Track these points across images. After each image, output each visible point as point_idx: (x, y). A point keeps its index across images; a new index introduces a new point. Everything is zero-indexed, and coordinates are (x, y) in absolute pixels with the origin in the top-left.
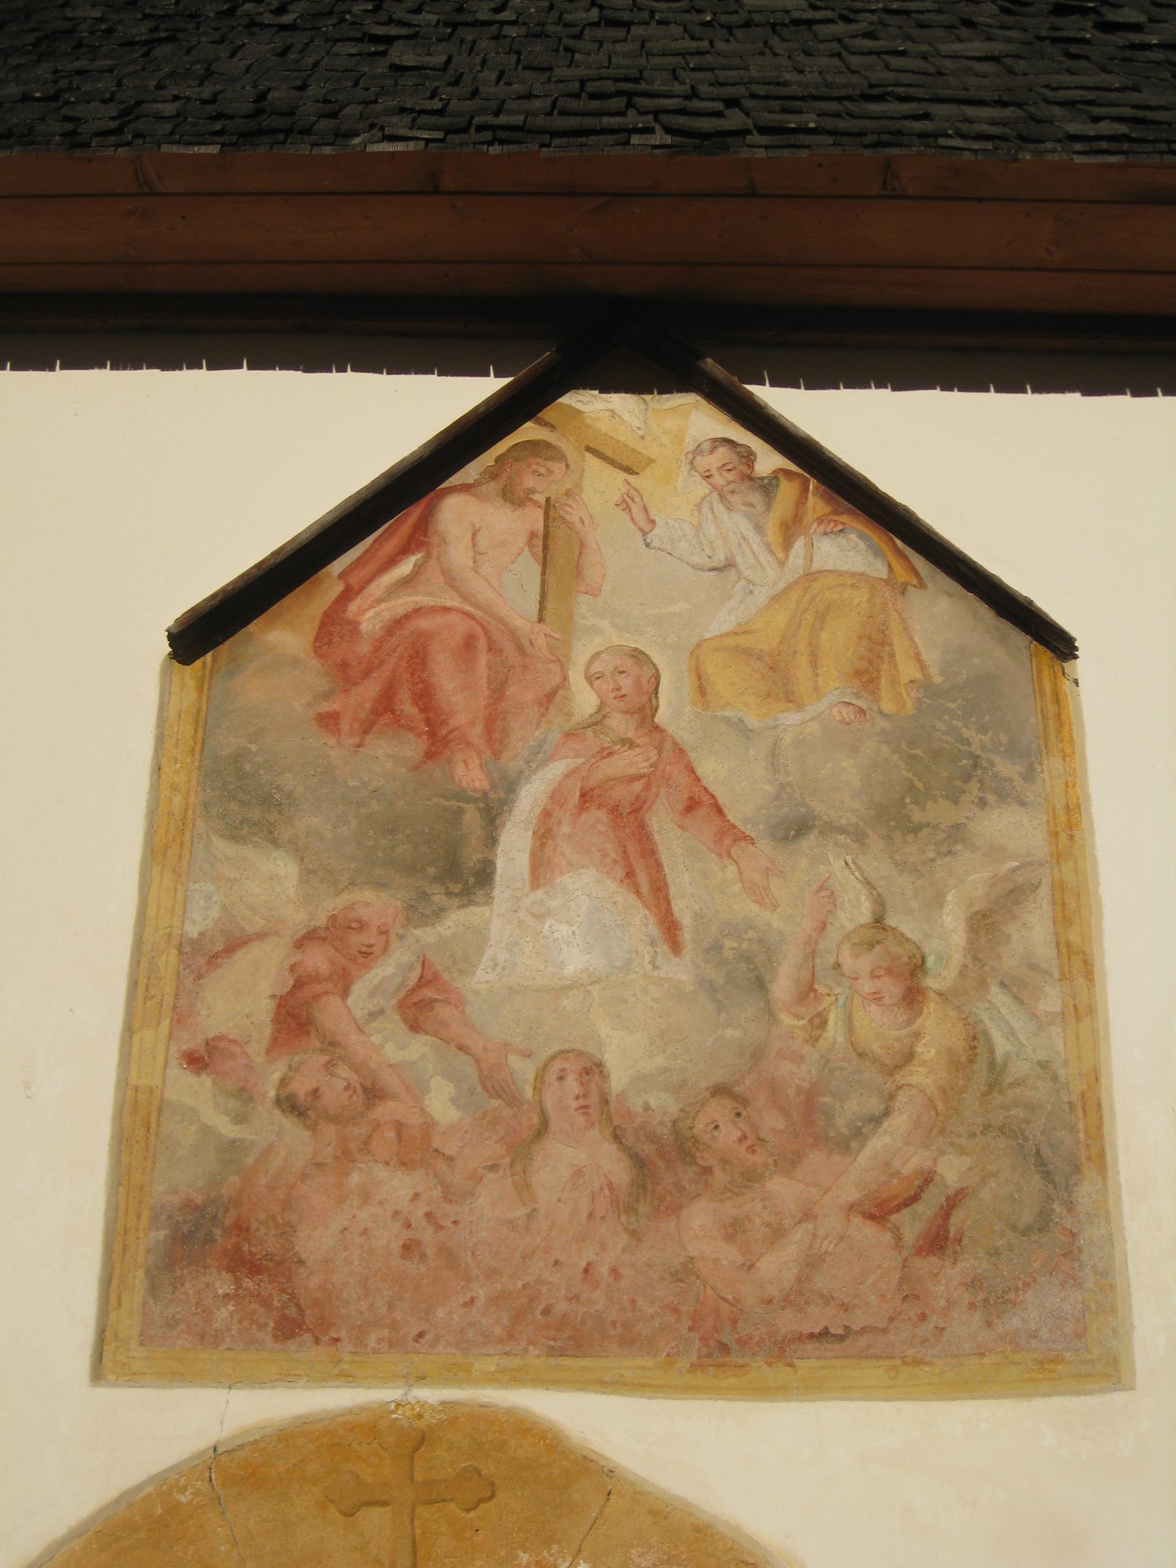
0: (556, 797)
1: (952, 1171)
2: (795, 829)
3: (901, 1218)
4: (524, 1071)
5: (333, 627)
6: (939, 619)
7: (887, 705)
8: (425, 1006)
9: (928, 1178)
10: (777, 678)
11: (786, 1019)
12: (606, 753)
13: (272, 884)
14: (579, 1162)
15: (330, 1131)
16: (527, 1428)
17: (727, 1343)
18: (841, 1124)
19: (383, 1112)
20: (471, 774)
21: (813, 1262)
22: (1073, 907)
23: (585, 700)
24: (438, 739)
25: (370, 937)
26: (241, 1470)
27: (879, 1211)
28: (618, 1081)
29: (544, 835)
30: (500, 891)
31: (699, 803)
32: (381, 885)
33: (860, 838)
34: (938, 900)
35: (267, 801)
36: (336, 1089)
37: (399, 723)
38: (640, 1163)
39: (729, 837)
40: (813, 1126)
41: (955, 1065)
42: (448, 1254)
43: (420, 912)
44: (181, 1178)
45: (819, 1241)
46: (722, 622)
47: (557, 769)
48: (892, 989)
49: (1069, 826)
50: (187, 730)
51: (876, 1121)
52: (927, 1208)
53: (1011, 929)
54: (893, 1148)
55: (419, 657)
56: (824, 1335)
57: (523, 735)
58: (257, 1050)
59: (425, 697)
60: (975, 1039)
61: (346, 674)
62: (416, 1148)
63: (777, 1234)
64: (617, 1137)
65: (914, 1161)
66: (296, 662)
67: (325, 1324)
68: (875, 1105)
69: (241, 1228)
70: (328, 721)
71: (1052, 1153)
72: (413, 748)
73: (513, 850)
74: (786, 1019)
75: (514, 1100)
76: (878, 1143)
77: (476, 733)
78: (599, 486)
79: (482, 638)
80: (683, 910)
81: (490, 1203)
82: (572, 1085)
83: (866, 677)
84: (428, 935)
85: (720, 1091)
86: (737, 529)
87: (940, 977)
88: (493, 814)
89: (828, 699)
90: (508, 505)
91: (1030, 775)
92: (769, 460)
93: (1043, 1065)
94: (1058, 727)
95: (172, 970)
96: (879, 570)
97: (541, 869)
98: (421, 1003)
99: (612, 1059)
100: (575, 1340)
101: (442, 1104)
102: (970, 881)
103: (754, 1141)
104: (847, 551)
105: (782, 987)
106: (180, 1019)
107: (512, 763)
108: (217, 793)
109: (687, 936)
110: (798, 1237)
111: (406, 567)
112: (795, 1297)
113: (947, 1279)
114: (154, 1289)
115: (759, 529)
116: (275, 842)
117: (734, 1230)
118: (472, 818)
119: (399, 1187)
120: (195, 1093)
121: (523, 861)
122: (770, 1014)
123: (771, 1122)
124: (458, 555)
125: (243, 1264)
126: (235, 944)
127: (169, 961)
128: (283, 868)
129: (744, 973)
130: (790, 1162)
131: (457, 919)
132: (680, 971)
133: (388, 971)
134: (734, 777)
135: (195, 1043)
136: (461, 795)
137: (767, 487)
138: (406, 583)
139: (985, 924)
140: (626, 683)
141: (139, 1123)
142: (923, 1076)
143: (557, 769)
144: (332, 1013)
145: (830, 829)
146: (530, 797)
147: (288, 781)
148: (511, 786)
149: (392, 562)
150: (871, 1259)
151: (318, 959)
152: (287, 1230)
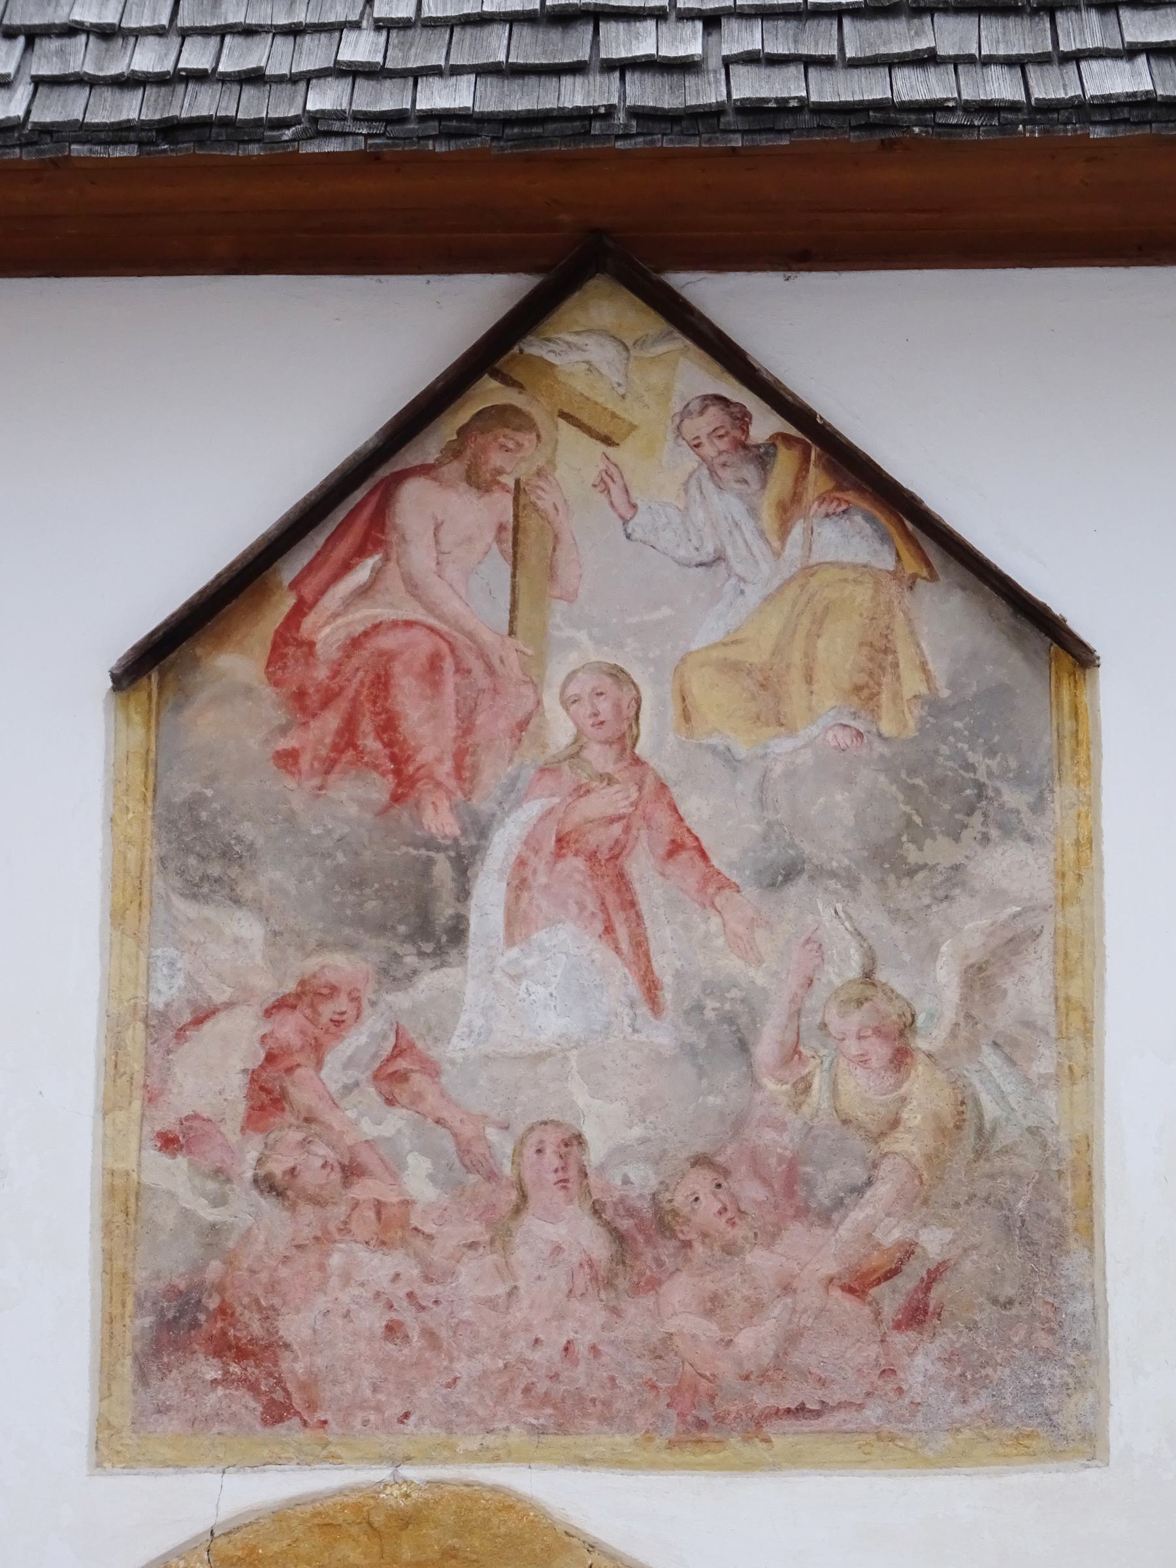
1: (934, 1242)
2: (784, 874)
5: (288, 643)
6: (943, 630)
10: (768, 693)
13: (238, 948)
14: (563, 1232)
16: (509, 1503)
22: (1077, 957)
27: (858, 1284)
29: (519, 885)
31: (682, 846)
39: (713, 883)
40: (795, 1195)
46: (710, 630)
54: (877, 1220)
55: (382, 683)
57: (493, 773)
59: (388, 726)
61: (303, 703)
62: (392, 1225)
72: (379, 788)
78: (574, 459)
81: (473, 1280)
83: (865, 693)
86: (729, 512)
88: (464, 865)
92: (765, 424)
94: (1077, 741)
95: (151, 1034)
97: (517, 924)
98: (398, 1072)
100: (563, 1412)
101: (419, 1181)
102: (969, 929)
104: (848, 540)
108: (185, 848)
113: (922, 1363)
117: (713, 1305)
119: (379, 1267)
120: (171, 1175)
124: (419, 555)
128: (249, 929)
129: (730, 1036)
130: (770, 1236)
132: (662, 1036)
133: (362, 1040)
134: (719, 816)
137: (763, 457)
139: (980, 979)
141: (123, 1206)
142: (909, 1144)
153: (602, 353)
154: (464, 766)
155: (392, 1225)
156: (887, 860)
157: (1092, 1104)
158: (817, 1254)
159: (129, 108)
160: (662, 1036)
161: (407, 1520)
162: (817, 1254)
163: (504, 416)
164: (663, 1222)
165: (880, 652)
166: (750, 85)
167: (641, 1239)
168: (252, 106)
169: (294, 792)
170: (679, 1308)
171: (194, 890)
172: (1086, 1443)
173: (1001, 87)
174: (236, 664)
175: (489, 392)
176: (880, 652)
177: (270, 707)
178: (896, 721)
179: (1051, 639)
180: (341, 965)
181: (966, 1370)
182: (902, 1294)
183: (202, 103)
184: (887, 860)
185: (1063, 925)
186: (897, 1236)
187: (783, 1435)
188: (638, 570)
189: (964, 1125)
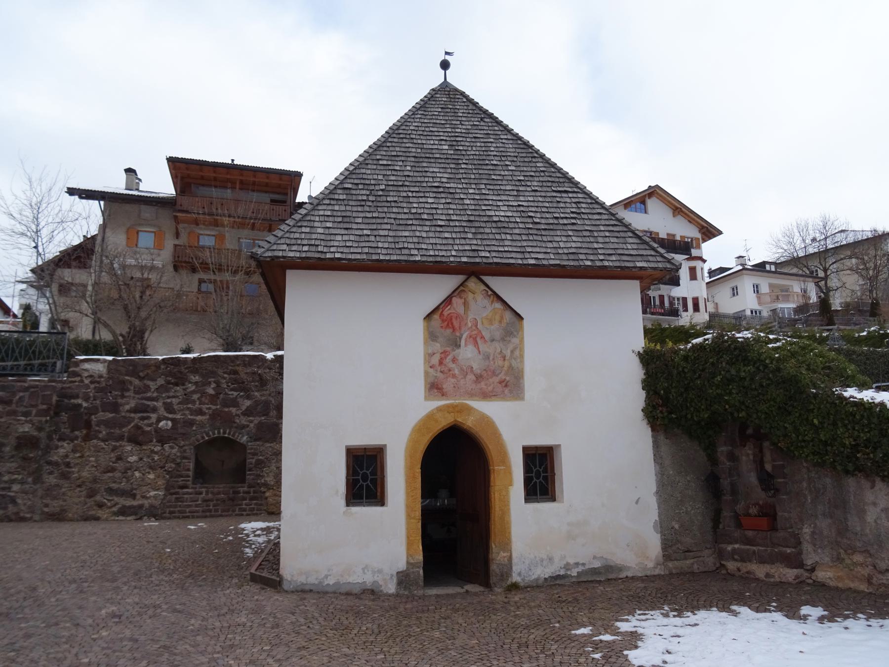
1: (508, 378)
2: (493, 340)
5: (441, 314)
6: (508, 315)
10: (491, 322)
13: (437, 347)
14: (471, 377)
16: (466, 404)
17: (485, 396)
22: (522, 350)
23: (470, 325)
24: (454, 330)
26: (439, 409)
27: (500, 383)
29: (466, 341)
31: (482, 337)
36: (446, 369)
39: (485, 341)
40: (494, 374)
45: (527, 612)
46: (484, 315)
49: (522, 341)
54: (502, 376)
55: (451, 319)
57: (463, 329)
59: (452, 324)
61: (443, 321)
62: (454, 376)
72: (451, 330)
73: (463, 342)
78: (470, 296)
79: (458, 316)
81: (462, 382)
83: (500, 322)
86: (486, 302)
87: (507, 358)
88: (460, 338)
89: (496, 325)
90: (369, 586)
92: (490, 292)
94: (522, 328)
95: (429, 356)
97: (466, 345)
98: (454, 360)
100: (471, 395)
101: (457, 372)
102: (511, 347)
104: (498, 305)
108: (431, 336)
112: (492, 392)
113: (507, 391)
117: (486, 385)
119: (453, 380)
120: (431, 370)
124: (455, 305)
128: (438, 345)
129: (487, 357)
130: (491, 378)
131: (457, 351)
132: (481, 357)
133: (450, 357)
134: (487, 336)
137: (489, 296)
139: (512, 352)
141: (426, 374)
142: (505, 368)
146: (464, 336)
151: (443, 356)
153: (473, 284)
154: (460, 328)
155: (454, 376)
156: (503, 339)
157: (523, 365)
158: (496, 380)
159: (431, 259)
160: (481, 357)
161: (456, 406)
162: (496, 380)
163: (463, 291)
164: (481, 376)
165: (502, 318)
166: (496, 260)
167: (479, 378)
168: (443, 259)
169: (442, 330)
170: (483, 385)
171: (433, 340)
172: (522, 399)
173: (520, 262)
174: (436, 316)
175: (462, 288)
176: (502, 318)
177: (439, 321)
178: (504, 325)
179: (520, 317)
180: (448, 349)
181: (511, 392)
182: (504, 384)
183: (439, 259)
184: (503, 339)
185: (520, 347)
186: (27, 430)
187: (493, 398)
188: (478, 308)
189: (511, 367)
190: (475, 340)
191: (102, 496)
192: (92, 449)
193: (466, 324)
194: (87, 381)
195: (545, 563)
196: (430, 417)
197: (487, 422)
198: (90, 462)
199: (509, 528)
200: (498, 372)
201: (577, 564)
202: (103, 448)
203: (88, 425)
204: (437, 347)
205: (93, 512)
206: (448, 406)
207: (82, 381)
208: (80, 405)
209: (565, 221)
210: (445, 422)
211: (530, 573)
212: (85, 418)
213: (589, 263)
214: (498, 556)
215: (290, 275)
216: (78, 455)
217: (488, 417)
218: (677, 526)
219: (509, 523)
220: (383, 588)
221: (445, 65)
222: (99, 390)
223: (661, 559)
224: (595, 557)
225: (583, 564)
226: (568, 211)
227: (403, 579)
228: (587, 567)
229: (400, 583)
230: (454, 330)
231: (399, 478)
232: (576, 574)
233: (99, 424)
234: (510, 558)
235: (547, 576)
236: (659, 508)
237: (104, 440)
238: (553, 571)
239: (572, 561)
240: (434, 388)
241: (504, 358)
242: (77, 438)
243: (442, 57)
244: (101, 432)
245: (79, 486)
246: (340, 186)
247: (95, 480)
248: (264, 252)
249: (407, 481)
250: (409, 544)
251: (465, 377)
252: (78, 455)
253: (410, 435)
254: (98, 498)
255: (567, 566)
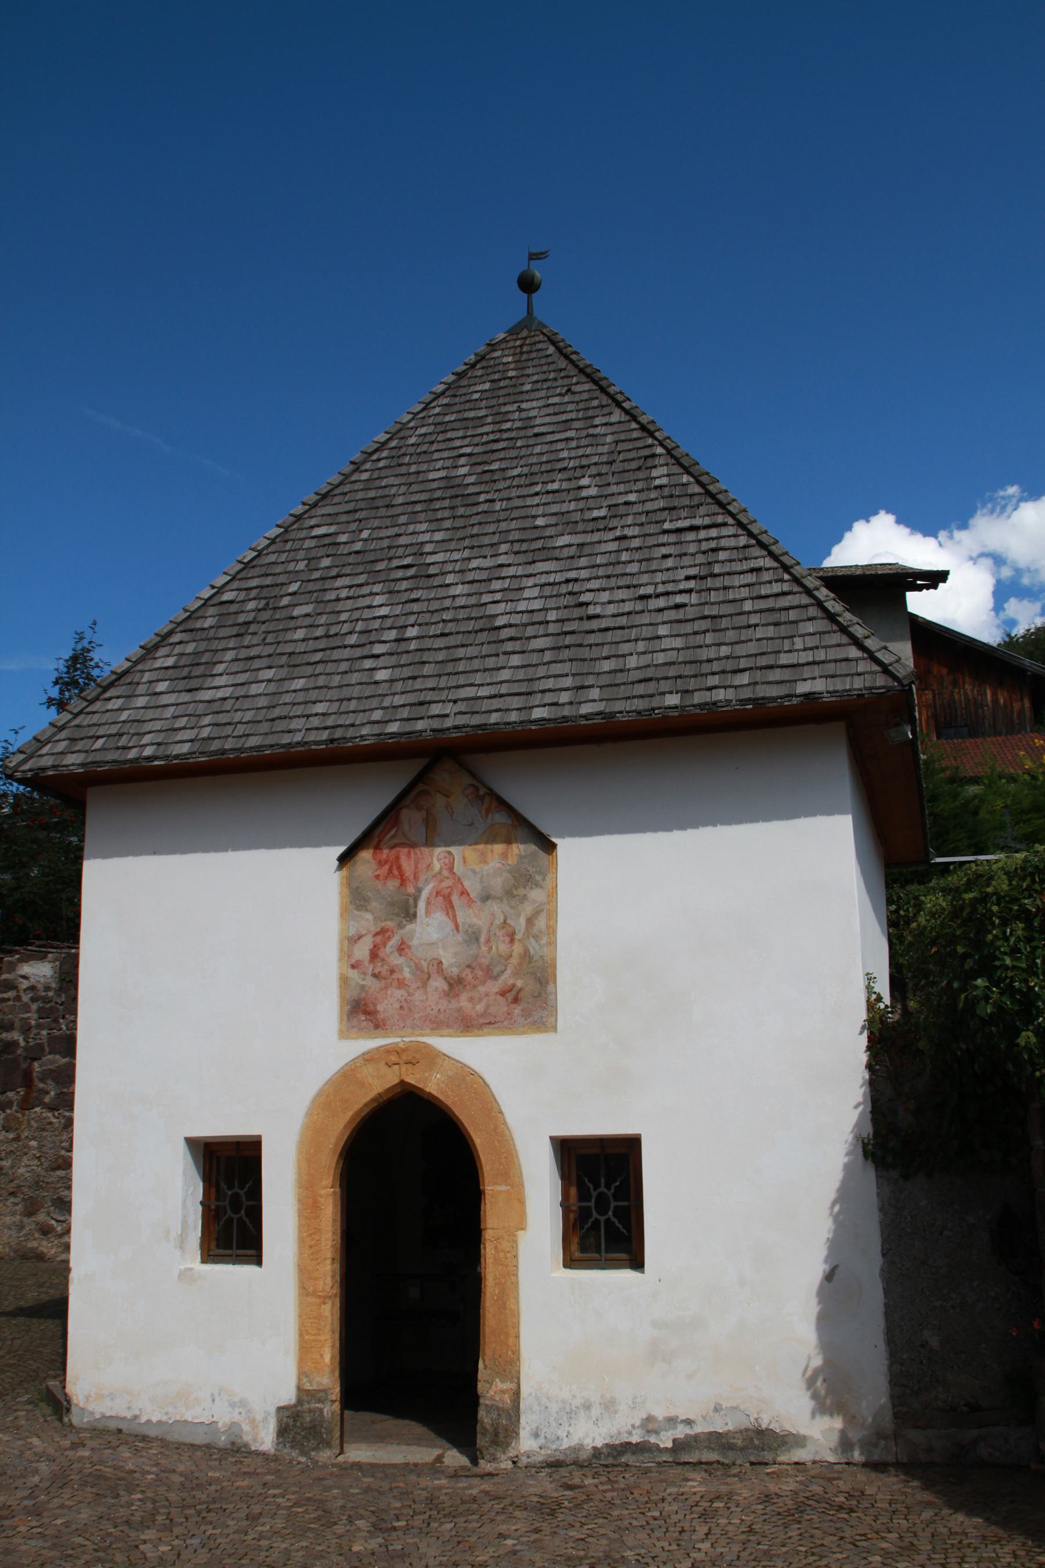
0: (430, 894)
1: (519, 983)
2: (486, 898)
3: (508, 995)
4: (425, 964)
7: (510, 862)
8: (403, 949)
9: (514, 985)
11: (483, 948)
12: (441, 881)
13: (367, 922)
14: (438, 984)
15: (383, 982)
17: (468, 1025)
18: (495, 973)
19: (395, 976)
20: (411, 890)
21: (488, 1006)
24: (403, 881)
25: (390, 933)
26: (368, 1058)
27: (503, 993)
28: (445, 965)
30: (418, 920)
31: (464, 893)
32: (392, 920)
33: (501, 900)
34: (519, 915)
35: (365, 900)
37: (394, 876)
38: (450, 985)
40: (490, 974)
41: (521, 958)
42: (410, 1009)
43: (401, 926)
44: (354, 994)
47: (431, 885)
48: (507, 939)
49: (553, 894)
50: (345, 881)
51: (503, 972)
52: (513, 993)
53: (536, 922)
54: (507, 978)
56: (490, 1023)
57: (422, 877)
58: (366, 963)
59: (399, 868)
60: (526, 951)
62: (401, 984)
63: (480, 1000)
64: (445, 979)
65: (511, 982)
66: (369, 862)
67: (384, 1025)
68: (503, 968)
69: (365, 1004)
70: (377, 877)
71: (542, 976)
73: (422, 905)
74: (483, 948)
75: (422, 971)
76: (503, 977)
77: (411, 878)
80: (459, 920)
81: (418, 996)
82: (435, 967)
84: (403, 932)
85: (468, 966)
88: (416, 899)
91: (544, 879)
93: (542, 957)
95: (352, 940)
96: (509, 822)
97: (428, 913)
98: (402, 948)
99: (444, 961)
100: (438, 1024)
101: (407, 973)
102: (528, 909)
103: (475, 978)
105: (482, 939)
106: (349, 956)
107: (420, 885)
109: (461, 928)
110: (485, 1000)
111: (393, 832)
113: (517, 1010)
114: (349, 1019)
115: (480, 812)
116: (367, 910)
117: (471, 1000)
118: (411, 901)
119: (399, 993)
120: (353, 974)
121: (423, 911)
122: (480, 947)
123: (480, 973)
125: (367, 1013)
126: (360, 937)
127: (346, 942)
128: (369, 916)
129: (473, 937)
130: (483, 983)
131: (409, 927)
133: (394, 942)
134: (472, 886)
135: (353, 961)
136: (409, 895)
137: (482, 799)
138: (393, 836)
139: (530, 921)
140: (447, 861)
141: (344, 980)
142: (514, 961)
143: (431, 885)
144: (381, 954)
145: (494, 898)
146: (425, 894)
147: (369, 894)
148: (419, 891)
149: (390, 831)
150: (501, 1007)
151: (379, 939)
152: (375, 1005)
154: (416, 877)
155: (401, 984)
156: (509, 894)
158: (493, 987)
160: (460, 938)
162: (493, 987)
167: (455, 985)
169: (379, 884)
170: (464, 1001)
175: (421, 787)
180: (389, 924)
185: (549, 909)
189: (526, 955)
190: (448, 899)
191: (48, 1214)
192: (34, 1124)
193: (429, 866)
194: (26, 998)
195: (595, 1411)
196: (348, 1076)
197: (469, 1079)
198: (30, 1148)
199: (517, 1326)
200: (496, 970)
201: (672, 1421)
202: (51, 1123)
203: (27, 1080)
204: (367, 922)
205: (35, 1244)
206: (388, 1050)
207: (18, 998)
208: (15, 1043)
209: (661, 602)
210: (380, 1082)
211: (561, 1433)
212: (24, 1066)
213: (673, 700)
214: (491, 1389)
215: (91, 792)
216: (11, 1136)
217: (473, 1073)
218: (935, 1342)
219: (516, 1314)
220: (247, 1438)
221: (528, 285)
222: (42, 1013)
223: (887, 1422)
224: (717, 1409)
225: (689, 1422)
226: (682, 574)
227: (295, 1424)
228: (698, 1429)
229: (282, 1431)
230: (403, 881)
231: (289, 1202)
232: (669, 1444)
233: (44, 1076)
234: (517, 1393)
235: (599, 1444)
236: (886, 1292)
237: (52, 1108)
238: (614, 1431)
239: (660, 1413)
240: (360, 1011)
241: (512, 937)
242: (9, 1104)
243: (521, 265)
244: (47, 1093)
245: (13, 1194)
246: (215, 601)
247: (37, 1184)
248: (24, 761)
249: (301, 1215)
250: (305, 1349)
251: (425, 985)
252: (11, 1136)
253: (309, 1114)
254: (41, 1217)
255: (649, 1423)
